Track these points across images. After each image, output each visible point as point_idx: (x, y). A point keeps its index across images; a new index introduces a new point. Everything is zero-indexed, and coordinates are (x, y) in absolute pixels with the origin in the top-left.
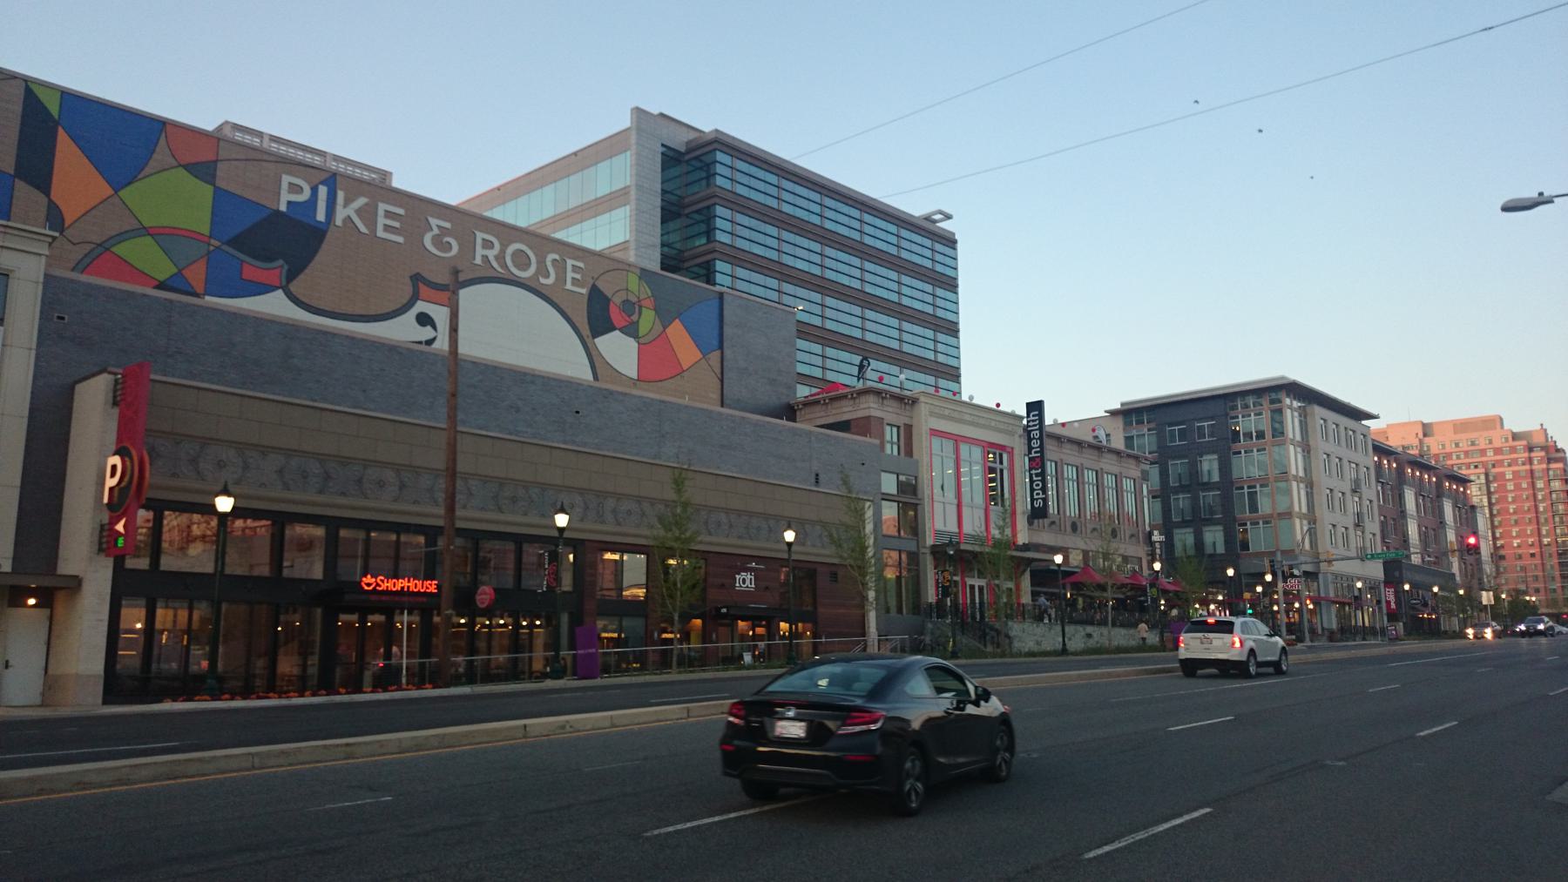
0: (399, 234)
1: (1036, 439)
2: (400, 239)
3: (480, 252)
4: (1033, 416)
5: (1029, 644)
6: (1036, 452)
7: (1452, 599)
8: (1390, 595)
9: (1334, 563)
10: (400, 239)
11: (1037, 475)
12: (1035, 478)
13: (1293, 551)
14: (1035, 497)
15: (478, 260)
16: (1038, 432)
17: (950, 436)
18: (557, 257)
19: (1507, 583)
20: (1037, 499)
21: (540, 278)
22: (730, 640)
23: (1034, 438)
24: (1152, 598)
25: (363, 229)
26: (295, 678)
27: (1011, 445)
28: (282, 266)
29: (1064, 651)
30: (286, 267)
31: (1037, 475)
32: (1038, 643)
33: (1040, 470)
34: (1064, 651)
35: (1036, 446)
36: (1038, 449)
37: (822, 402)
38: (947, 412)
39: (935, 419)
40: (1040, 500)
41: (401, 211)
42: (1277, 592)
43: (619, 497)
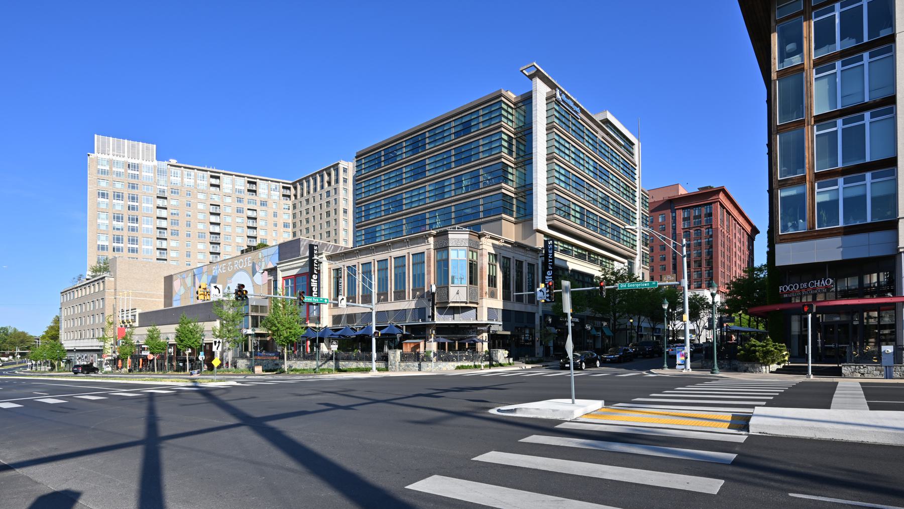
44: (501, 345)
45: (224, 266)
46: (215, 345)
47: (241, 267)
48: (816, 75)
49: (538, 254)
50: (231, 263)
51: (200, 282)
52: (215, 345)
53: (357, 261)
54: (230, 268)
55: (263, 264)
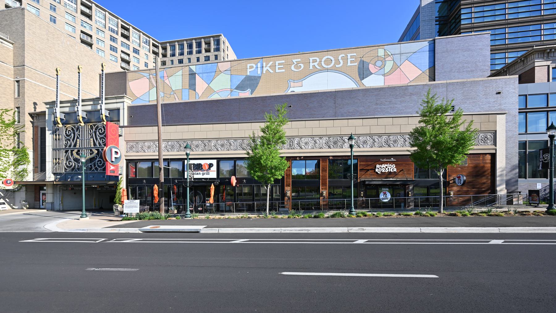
0: (283, 69)
2: (284, 70)
3: (311, 64)
7: (480, 158)
10: (284, 70)
15: (311, 68)
18: (344, 55)
21: (336, 65)
22: (435, 177)
24: (543, 163)
25: (272, 71)
26: (238, 189)
27: (434, 18)
28: (249, 90)
29: (518, 204)
30: (250, 90)
34: (518, 204)
37: (502, 71)
41: (283, 61)
42: (81, 174)
43: (301, 137)
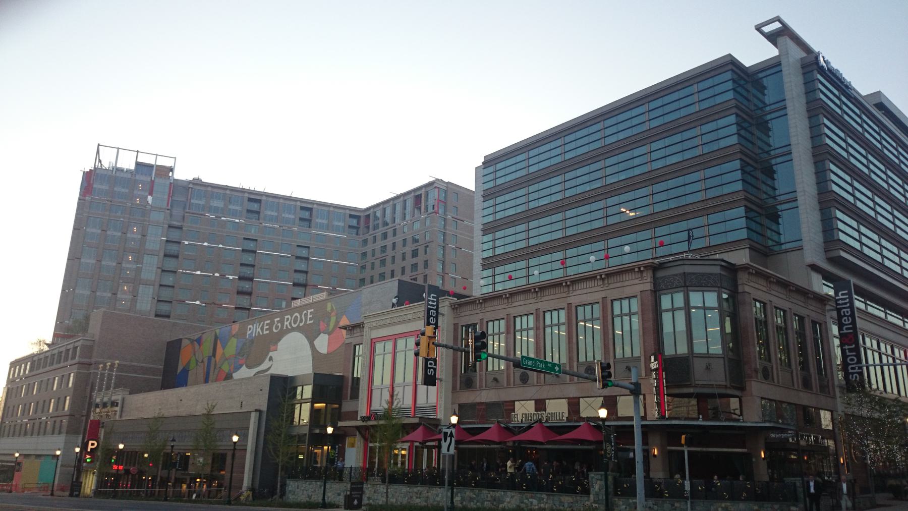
1: (848, 316)
4: (842, 295)
5: (302, 498)
6: (847, 329)
8: (348, 493)
9: (825, 59)
11: (850, 350)
12: (848, 354)
13: (413, 251)
14: (429, 366)
16: (849, 310)
17: (388, 338)
19: (509, 503)
20: (853, 373)
23: (845, 316)
31: (850, 350)
32: (310, 497)
33: (853, 346)
35: (847, 323)
36: (851, 326)
38: (388, 321)
39: (375, 331)
40: (432, 370)
44: (387, 480)
45: (267, 325)
46: (445, 441)
47: (294, 326)
48: (421, 194)
49: (825, 305)
50: (278, 319)
51: (223, 350)
52: (445, 441)
53: (480, 316)
54: (277, 327)
55: (333, 319)
